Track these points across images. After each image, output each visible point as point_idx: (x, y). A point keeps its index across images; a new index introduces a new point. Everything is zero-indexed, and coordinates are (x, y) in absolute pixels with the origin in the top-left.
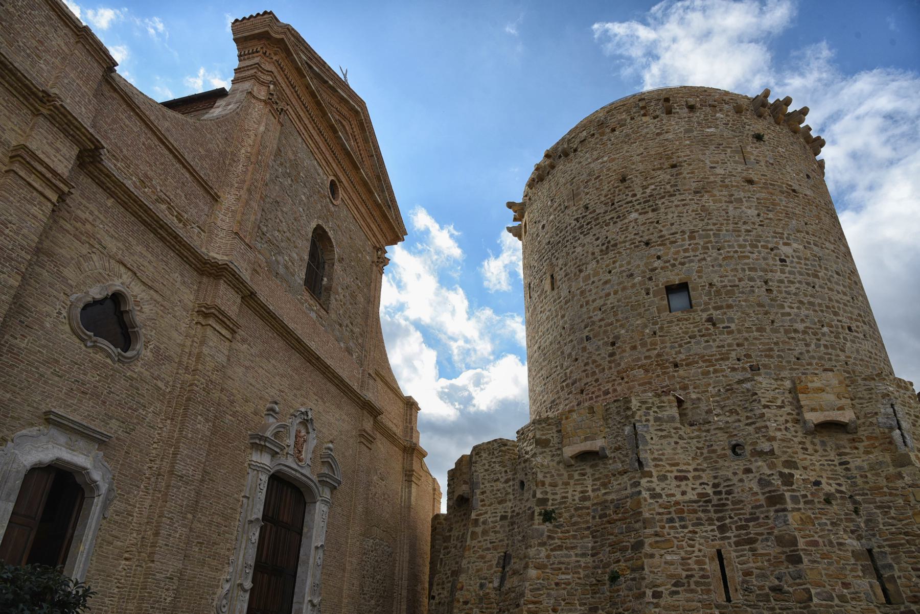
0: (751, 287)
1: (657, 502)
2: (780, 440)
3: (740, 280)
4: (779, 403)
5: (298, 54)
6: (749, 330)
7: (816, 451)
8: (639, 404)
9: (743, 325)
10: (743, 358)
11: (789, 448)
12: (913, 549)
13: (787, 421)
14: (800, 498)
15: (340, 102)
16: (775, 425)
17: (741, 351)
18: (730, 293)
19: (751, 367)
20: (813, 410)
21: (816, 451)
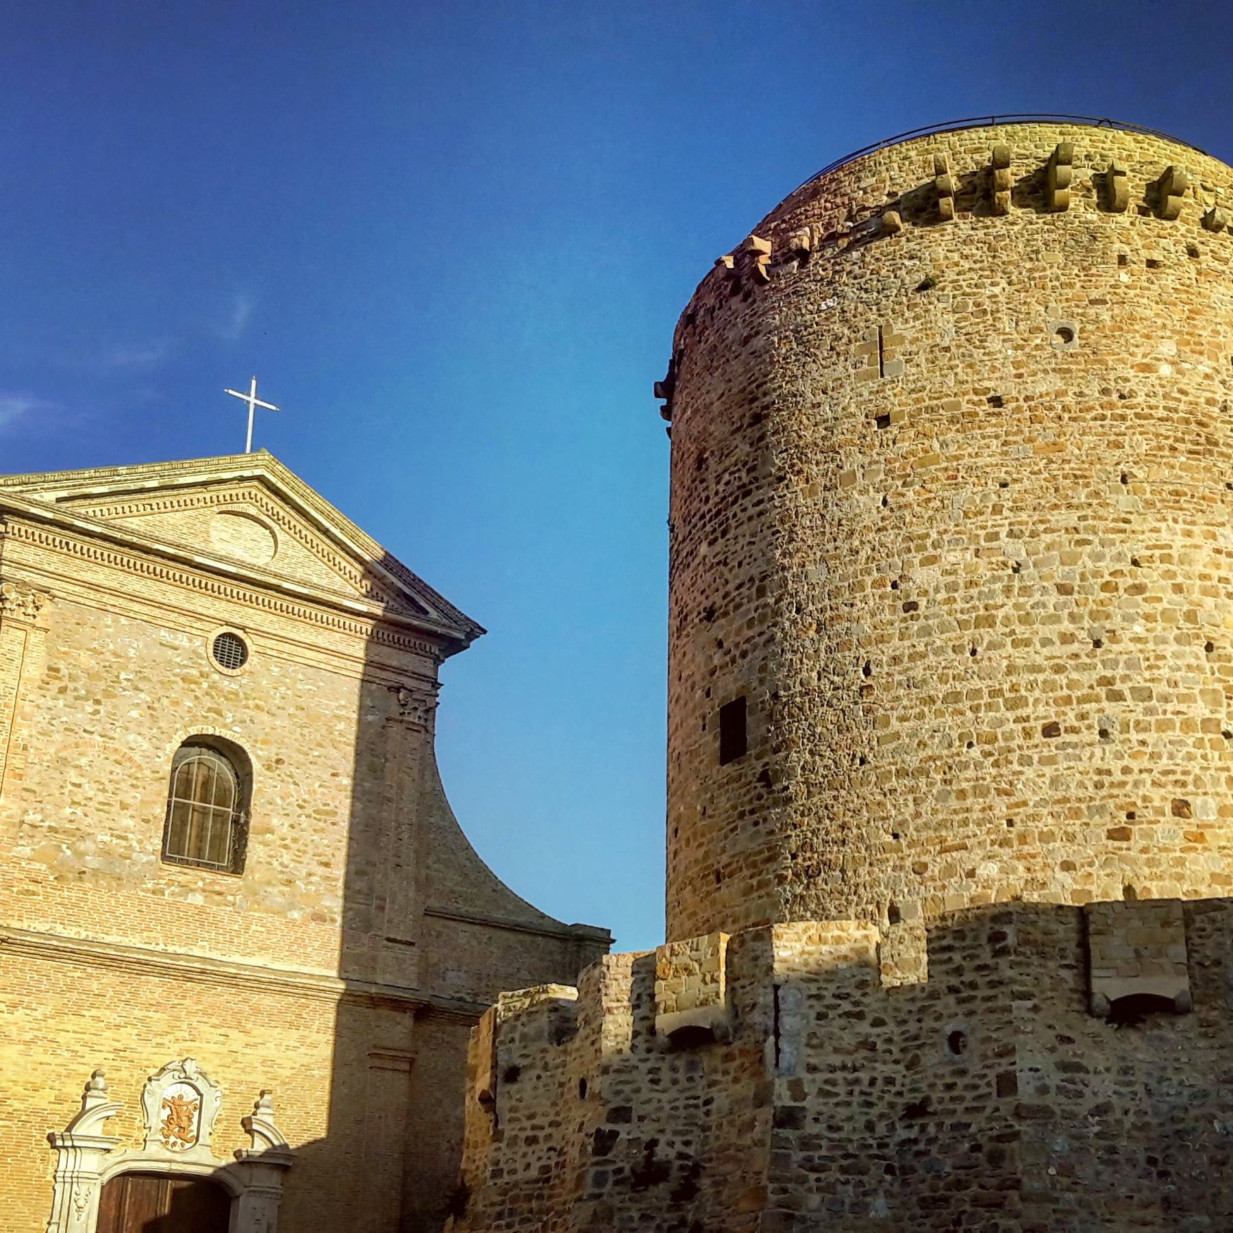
7: (675, 1082)
11: (628, 1082)
14: (611, 1175)
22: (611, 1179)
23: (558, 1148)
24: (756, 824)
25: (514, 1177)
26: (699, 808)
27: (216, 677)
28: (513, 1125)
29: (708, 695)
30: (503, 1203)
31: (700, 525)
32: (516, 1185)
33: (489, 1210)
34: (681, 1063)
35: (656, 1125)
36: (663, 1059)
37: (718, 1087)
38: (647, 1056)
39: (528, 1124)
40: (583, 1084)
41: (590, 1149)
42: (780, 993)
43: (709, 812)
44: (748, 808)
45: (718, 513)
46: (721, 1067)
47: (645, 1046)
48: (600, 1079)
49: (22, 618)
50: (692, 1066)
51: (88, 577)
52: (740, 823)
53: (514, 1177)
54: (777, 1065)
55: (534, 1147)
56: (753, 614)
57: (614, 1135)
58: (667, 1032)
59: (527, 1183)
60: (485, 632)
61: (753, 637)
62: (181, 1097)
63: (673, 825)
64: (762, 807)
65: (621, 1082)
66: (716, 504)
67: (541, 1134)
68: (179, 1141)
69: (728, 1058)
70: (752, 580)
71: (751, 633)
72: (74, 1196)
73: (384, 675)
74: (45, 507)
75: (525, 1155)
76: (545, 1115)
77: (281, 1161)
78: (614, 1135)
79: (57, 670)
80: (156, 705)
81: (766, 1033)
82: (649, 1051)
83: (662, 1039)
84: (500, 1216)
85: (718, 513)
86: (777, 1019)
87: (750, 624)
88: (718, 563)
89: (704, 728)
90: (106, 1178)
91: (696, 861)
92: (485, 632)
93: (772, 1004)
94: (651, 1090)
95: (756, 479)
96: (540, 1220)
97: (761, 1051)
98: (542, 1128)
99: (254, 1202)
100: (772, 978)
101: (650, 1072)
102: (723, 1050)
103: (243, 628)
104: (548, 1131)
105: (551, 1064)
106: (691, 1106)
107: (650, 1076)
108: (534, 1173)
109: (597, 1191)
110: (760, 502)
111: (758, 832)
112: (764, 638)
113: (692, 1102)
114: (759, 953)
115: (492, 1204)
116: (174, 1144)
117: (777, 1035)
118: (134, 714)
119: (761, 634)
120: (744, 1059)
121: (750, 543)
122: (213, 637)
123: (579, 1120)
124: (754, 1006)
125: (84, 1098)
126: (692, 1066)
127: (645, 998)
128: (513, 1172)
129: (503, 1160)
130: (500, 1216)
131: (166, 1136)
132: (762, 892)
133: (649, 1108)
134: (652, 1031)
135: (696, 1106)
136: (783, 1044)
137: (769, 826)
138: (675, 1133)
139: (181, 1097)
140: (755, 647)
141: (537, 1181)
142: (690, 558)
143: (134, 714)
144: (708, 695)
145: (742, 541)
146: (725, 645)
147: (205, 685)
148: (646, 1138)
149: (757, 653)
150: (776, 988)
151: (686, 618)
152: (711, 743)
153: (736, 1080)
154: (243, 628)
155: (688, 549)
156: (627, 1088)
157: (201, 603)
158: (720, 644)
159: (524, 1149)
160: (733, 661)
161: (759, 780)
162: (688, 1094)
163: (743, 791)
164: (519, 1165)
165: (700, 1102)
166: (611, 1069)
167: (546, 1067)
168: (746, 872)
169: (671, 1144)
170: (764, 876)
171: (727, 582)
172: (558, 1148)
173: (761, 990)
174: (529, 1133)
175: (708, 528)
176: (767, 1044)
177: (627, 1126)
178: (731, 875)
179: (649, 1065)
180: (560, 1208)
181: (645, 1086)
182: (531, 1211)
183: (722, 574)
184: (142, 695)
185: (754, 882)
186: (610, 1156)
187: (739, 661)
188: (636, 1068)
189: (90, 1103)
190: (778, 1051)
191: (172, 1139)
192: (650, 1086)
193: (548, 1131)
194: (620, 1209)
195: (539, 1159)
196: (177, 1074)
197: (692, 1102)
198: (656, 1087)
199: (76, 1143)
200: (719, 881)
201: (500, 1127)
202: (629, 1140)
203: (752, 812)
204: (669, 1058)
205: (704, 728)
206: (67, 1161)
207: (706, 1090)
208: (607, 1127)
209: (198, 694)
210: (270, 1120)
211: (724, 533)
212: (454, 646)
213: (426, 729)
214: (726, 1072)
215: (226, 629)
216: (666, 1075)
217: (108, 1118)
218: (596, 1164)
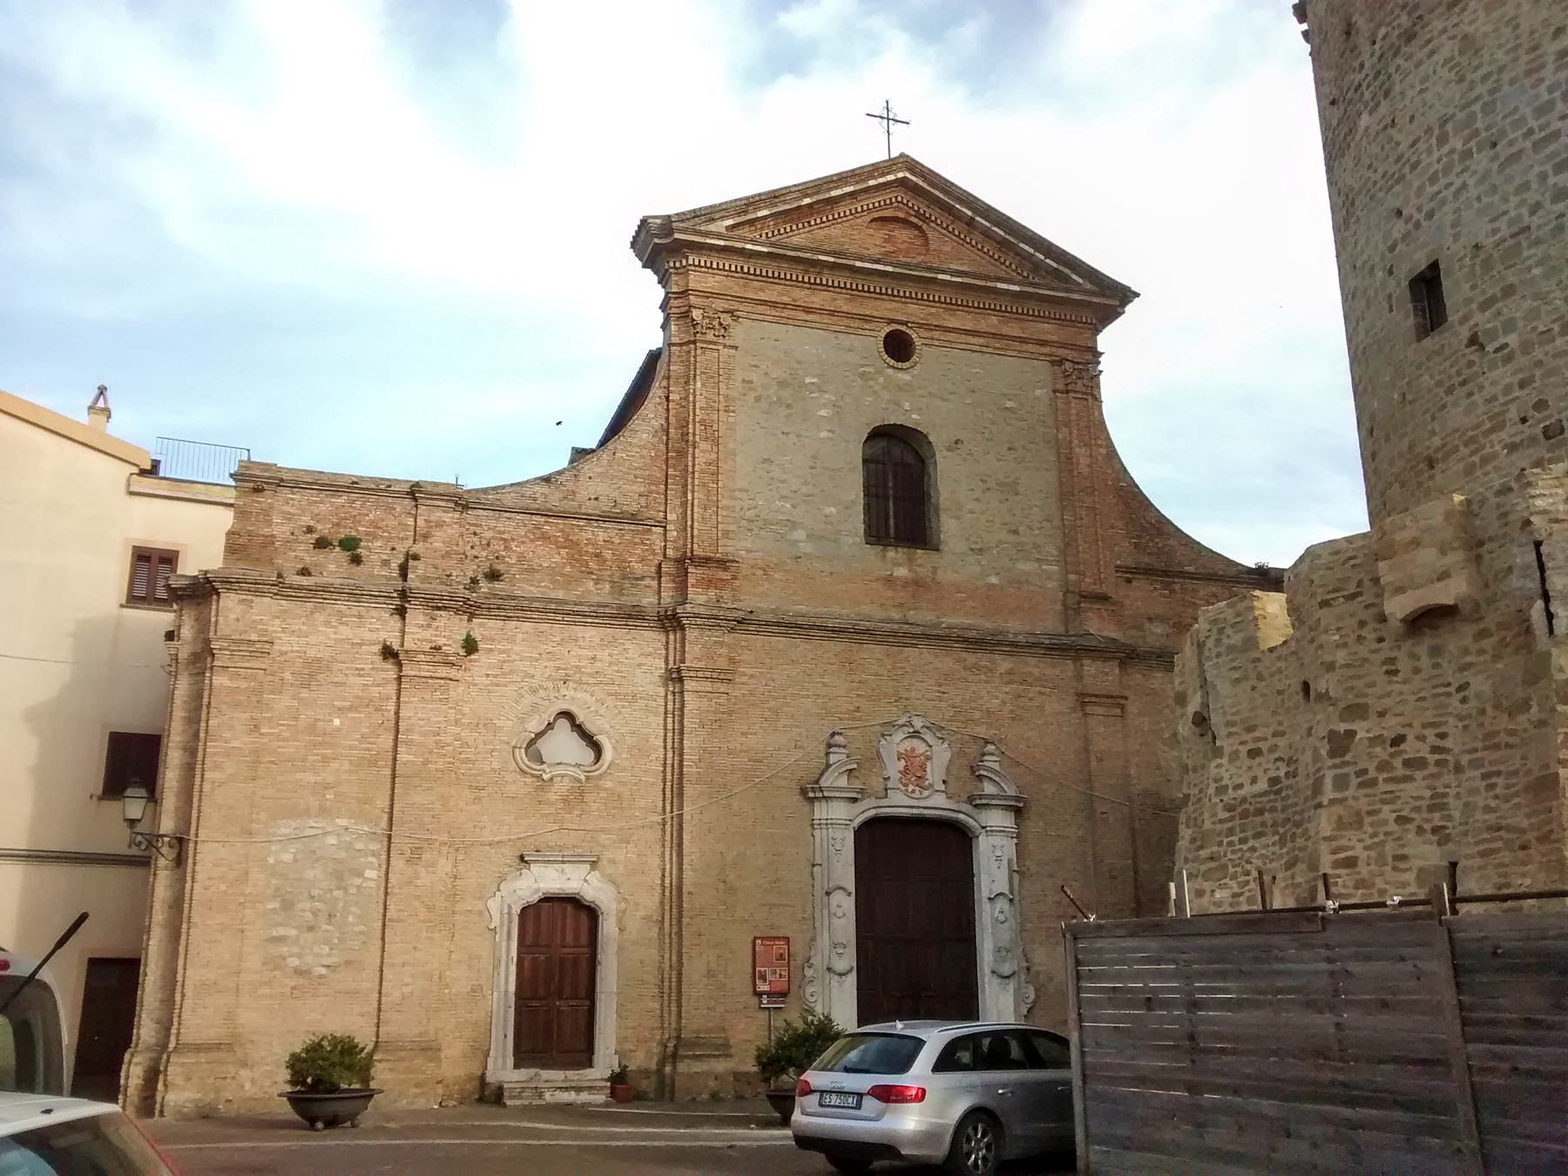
0: (1557, 218)
1: (1222, 800)
2: (1342, 666)
3: (1535, 208)
4: (1352, 589)
5: (707, 234)
6: (1547, 336)
7: (1417, 671)
8: (1208, 627)
9: (1535, 328)
10: (1531, 412)
11: (1359, 677)
12: (320, 1062)
13: (1362, 624)
14: (1353, 776)
15: (856, 198)
16: (1337, 637)
17: (1529, 396)
18: (1511, 256)
19: (1546, 431)
20: (1400, 590)
21: (1417, 671)
22: (1354, 781)
23: (1286, 758)
24: (1470, 394)
25: (1242, 792)
26: (1396, 396)
27: (890, 371)
28: (1231, 740)
29: (1391, 273)
30: (1232, 819)
31: (1356, 97)
32: (1244, 800)
33: (1219, 827)
34: (1422, 650)
35: (1399, 719)
36: (1399, 648)
37: (1472, 671)
38: (1378, 646)
39: (1248, 737)
40: (1306, 687)
41: (1323, 752)
42: (1543, 549)
43: (1409, 397)
44: (1456, 380)
45: (1378, 74)
46: (1474, 647)
47: (1373, 636)
48: (1327, 676)
49: (714, 339)
50: (1436, 651)
51: (763, 296)
52: (1450, 399)
53: (1242, 792)
54: (1551, 631)
55: (1258, 760)
56: (1437, 167)
57: (1351, 734)
58: (1400, 616)
59: (1255, 796)
60: (1137, 295)
61: (1439, 192)
62: (913, 750)
63: (1368, 425)
64: (1476, 375)
65: (1351, 677)
66: (1373, 66)
67: (1264, 746)
68: (917, 788)
69: (1482, 634)
70: (1429, 130)
71: (1436, 188)
72: (831, 841)
73: (1047, 350)
74: (719, 236)
75: (1250, 768)
76: (1267, 725)
77: (1013, 803)
78: (1351, 734)
79: (751, 382)
80: (840, 403)
81: (1532, 600)
82: (1381, 640)
83: (1395, 623)
84: (1231, 832)
85: (1378, 74)
86: (1543, 580)
87: (1433, 179)
88: (1385, 128)
89: (1391, 310)
90: (856, 823)
91: (1401, 454)
92: (1137, 295)
93: (1535, 564)
94: (1389, 682)
95: (1420, 17)
96: (1277, 833)
97: (1528, 620)
98: (1266, 739)
99: (997, 840)
100: (1531, 533)
101: (1384, 663)
102: (1474, 628)
103: (905, 323)
104: (1272, 741)
105: (1265, 674)
106: (1441, 695)
107: (1385, 668)
108: (1263, 785)
109: (1338, 795)
110: (1429, 41)
111: (1474, 404)
112: (1453, 189)
113: (1442, 690)
114: (1507, 508)
115: (1221, 821)
116: (913, 791)
117: (1546, 597)
118: (823, 413)
119: (1448, 185)
120: (1503, 633)
121: (1422, 91)
122: (883, 334)
123: (1306, 726)
124: (1510, 570)
125: (827, 754)
126: (1436, 651)
127: (1367, 583)
128: (1241, 786)
129: (1226, 776)
130: (1231, 832)
131: (906, 785)
132: (1489, 468)
133: (1388, 702)
134: (1382, 618)
135: (1448, 695)
136: (1555, 607)
137: (1486, 393)
138: (1424, 726)
139: (913, 750)
140: (1443, 202)
141: (1265, 794)
142: (1349, 138)
143: (823, 413)
144: (1391, 273)
145: (1410, 94)
146: (1405, 212)
147: (881, 380)
148: (1389, 735)
149: (1446, 208)
150: (1538, 544)
151: (1353, 204)
152: (1405, 319)
153: (1497, 657)
154: (905, 323)
155: (1346, 129)
156: (1359, 684)
157: (869, 308)
158: (1399, 213)
159: (1248, 762)
160: (1418, 225)
161: (1468, 346)
162: (1435, 682)
163: (1447, 364)
164: (1246, 779)
165: (1452, 689)
166: (1338, 665)
167: (1260, 677)
168: (1464, 451)
169: (1421, 738)
170: (1487, 450)
171: (1398, 144)
172: (1286, 758)
173: (1515, 550)
174: (1251, 746)
175: (1367, 95)
176: (1533, 612)
177: (1365, 724)
178: (1445, 458)
179: (1381, 656)
180: (1297, 817)
181: (1381, 679)
182: (1263, 824)
183: (1391, 138)
184: (827, 396)
185: (1476, 459)
186: (1348, 757)
187: (1425, 224)
188: (1365, 660)
189: (833, 758)
190: (1550, 616)
191: (911, 788)
192: (1386, 678)
193: (1272, 741)
194: (1370, 813)
195: (1266, 771)
196: (906, 729)
197: (1442, 690)
198: (1395, 679)
199: (826, 794)
200: (1432, 467)
201: (1218, 743)
202: (1369, 739)
203: (1464, 383)
204: (1407, 646)
205: (1391, 310)
206: (821, 811)
207: (1458, 675)
208: (1342, 727)
209: (877, 388)
210: (996, 766)
211: (1387, 94)
212: (1109, 314)
213: (1091, 393)
214: (1481, 652)
215: (894, 327)
216: (1404, 665)
217: (851, 770)
218: (1336, 766)
